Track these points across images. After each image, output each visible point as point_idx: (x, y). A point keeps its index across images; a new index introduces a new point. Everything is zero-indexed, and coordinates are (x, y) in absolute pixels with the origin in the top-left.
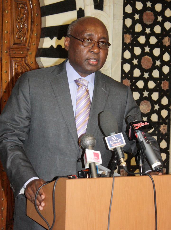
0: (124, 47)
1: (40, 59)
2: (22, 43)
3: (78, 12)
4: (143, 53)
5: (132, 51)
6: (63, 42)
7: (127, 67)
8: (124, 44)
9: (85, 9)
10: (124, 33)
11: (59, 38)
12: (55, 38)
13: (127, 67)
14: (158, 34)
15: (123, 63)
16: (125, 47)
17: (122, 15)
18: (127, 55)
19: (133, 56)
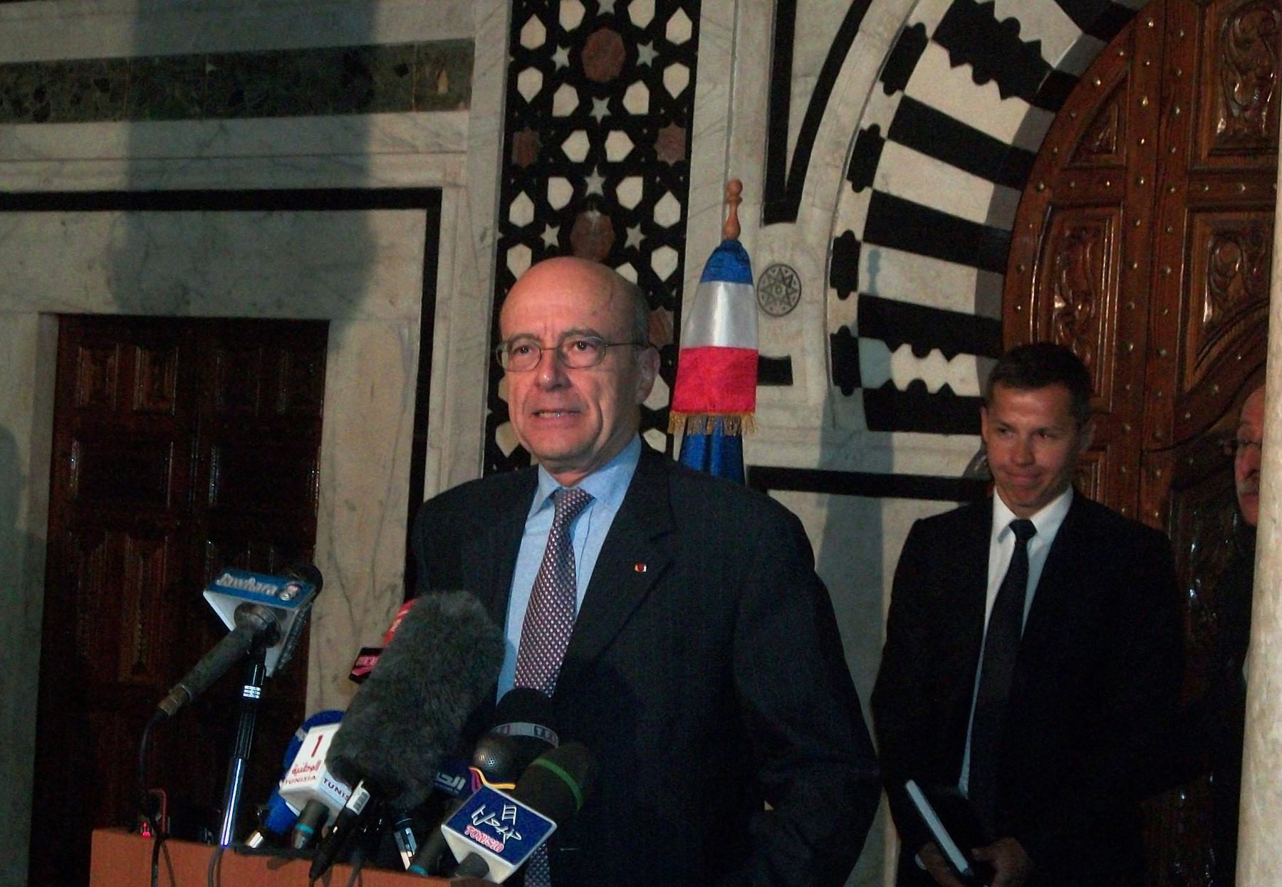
0: (674, 293)
1: (988, 218)
2: (1108, 90)
3: (902, 87)
4: (615, 92)
5: (658, 92)
6: (903, 367)
7: (666, 211)
8: (686, 122)
9: (873, 77)
10: (684, 167)
11: (918, 385)
12: (934, 386)
13: (666, 211)
14: (558, 174)
15: (681, 227)
16: (675, 112)
17: (701, 55)
18: (675, 79)
19: (653, 78)
